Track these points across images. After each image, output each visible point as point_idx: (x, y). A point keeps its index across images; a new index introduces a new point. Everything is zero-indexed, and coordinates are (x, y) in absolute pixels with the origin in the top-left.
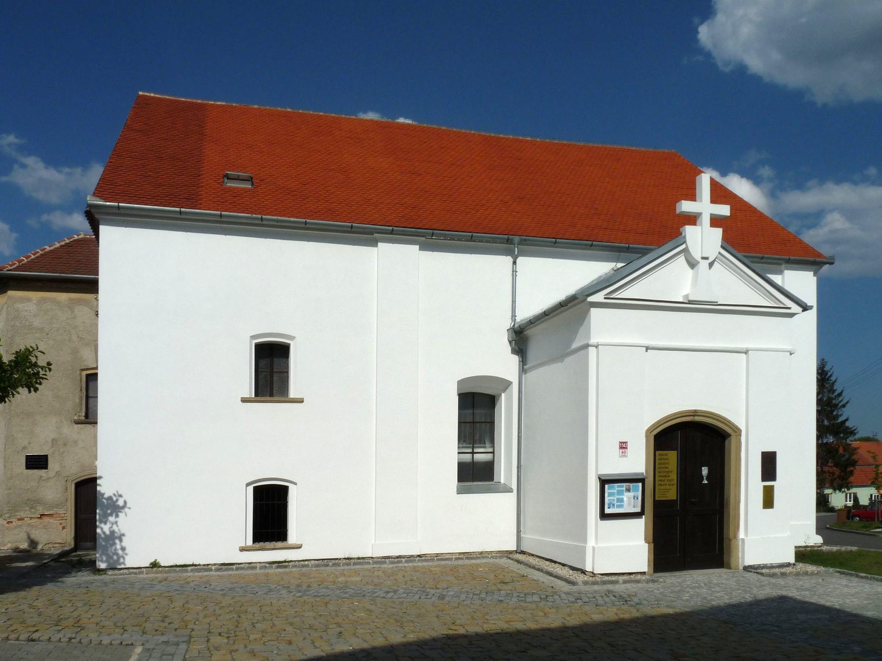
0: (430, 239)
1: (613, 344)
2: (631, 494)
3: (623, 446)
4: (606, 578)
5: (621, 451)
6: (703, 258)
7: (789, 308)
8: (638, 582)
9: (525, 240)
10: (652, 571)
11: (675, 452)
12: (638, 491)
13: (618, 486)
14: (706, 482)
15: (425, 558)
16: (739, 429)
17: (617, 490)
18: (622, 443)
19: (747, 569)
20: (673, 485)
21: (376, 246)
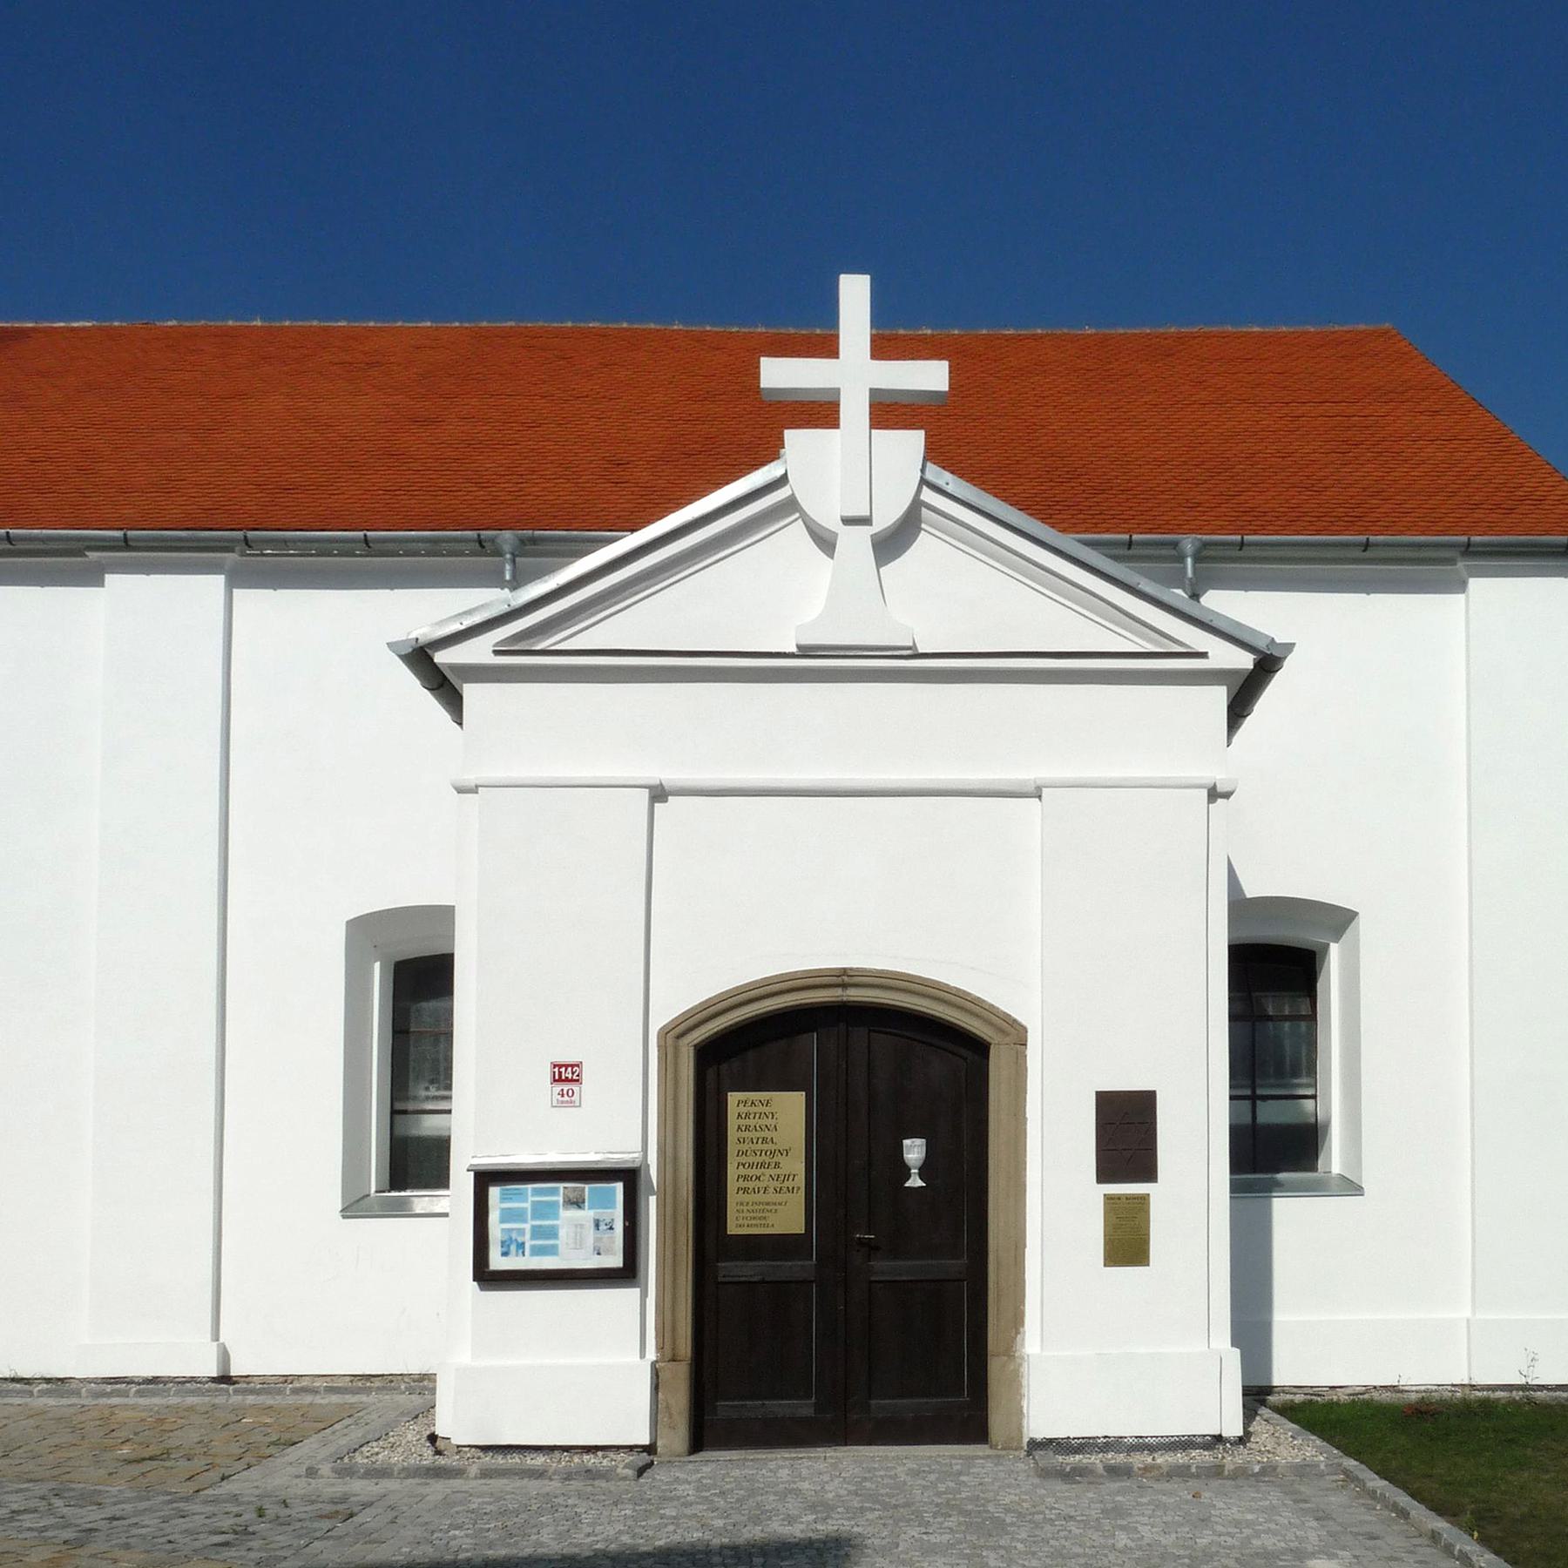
0: (257, 555)
1: (531, 782)
2: (587, 1215)
3: (566, 1075)
4: (500, 1460)
5: (558, 1088)
6: (848, 521)
7: (1203, 655)
8: (539, 1474)
9: (534, 541)
10: (676, 1437)
11: (799, 1097)
12: (612, 1205)
13: (536, 1192)
14: (920, 1183)
15: (245, 1386)
16: (1015, 1021)
17: (534, 1203)
18: (560, 1066)
19: (1035, 1445)
20: (791, 1190)
21: (100, 583)
